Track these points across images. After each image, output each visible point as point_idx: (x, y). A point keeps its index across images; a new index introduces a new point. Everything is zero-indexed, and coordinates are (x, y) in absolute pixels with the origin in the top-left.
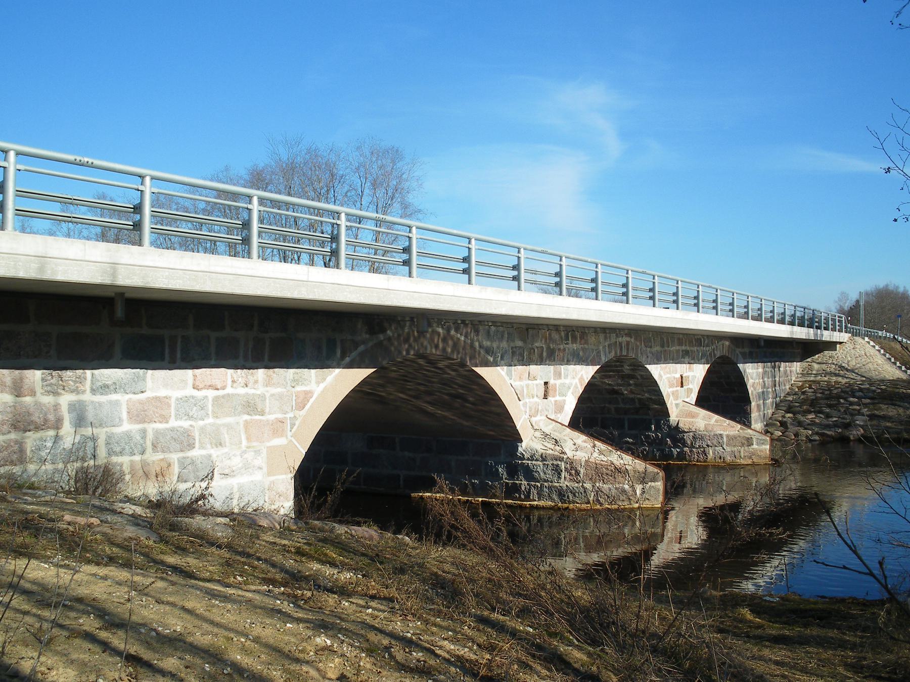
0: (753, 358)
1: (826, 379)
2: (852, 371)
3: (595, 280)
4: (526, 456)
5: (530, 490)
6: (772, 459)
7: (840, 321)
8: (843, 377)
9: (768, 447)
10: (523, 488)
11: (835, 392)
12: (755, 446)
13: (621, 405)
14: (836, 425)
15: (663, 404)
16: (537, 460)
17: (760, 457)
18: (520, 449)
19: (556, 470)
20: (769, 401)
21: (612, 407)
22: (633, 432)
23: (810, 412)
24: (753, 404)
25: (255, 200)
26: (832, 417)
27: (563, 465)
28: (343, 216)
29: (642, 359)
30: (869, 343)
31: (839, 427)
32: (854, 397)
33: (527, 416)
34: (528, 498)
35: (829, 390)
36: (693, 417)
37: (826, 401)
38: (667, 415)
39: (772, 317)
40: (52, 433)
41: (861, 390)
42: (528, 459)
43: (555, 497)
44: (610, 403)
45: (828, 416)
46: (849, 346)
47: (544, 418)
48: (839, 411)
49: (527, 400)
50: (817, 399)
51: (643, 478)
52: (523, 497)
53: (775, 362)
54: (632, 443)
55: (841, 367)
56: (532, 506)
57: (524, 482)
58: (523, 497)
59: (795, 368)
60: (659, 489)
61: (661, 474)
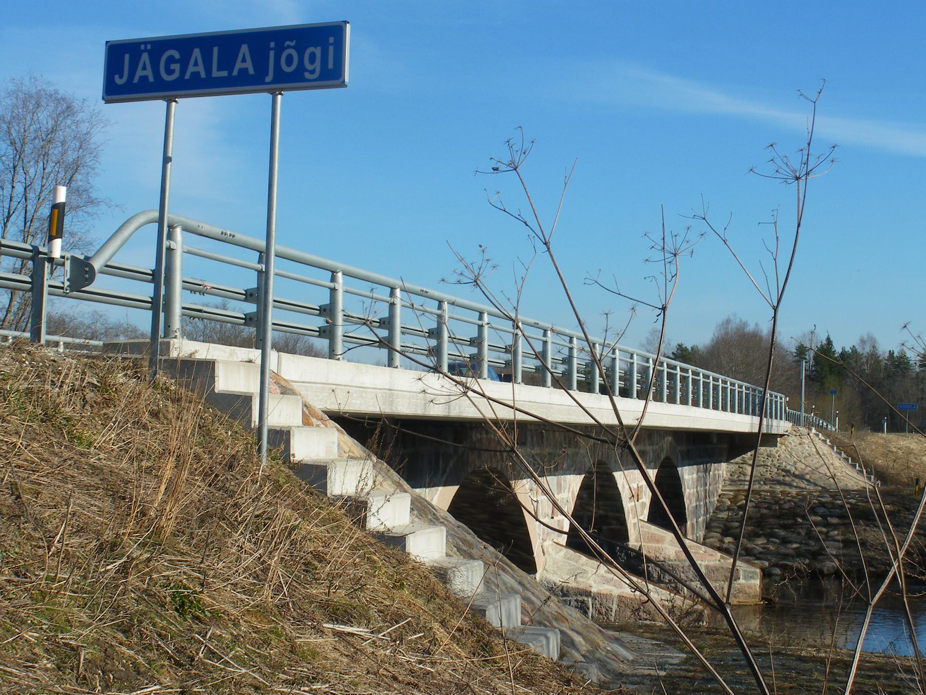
0: (690, 459)
1: (767, 487)
2: (801, 477)
3: (327, 311)
6: (763, 599)
7: (671, 377)
8: (790, 485)
9: (758, 582)
11: (787, 506)
12: (742, 581)
14: (798, 554)
15: (623, 522)
17: (748, 595)
20: (701, 519)
23: (758, 536)
24: (689, 523)
25: (665, 365)
26: (791, 542)
28: (665, 365)
30: (817, 435)
31: (806, 557)
32: (816, 514)
35: (777, 503)
36: (658, 541)
37: (777, 521)
38: (627, 538)
39: (567, 375)
41: (822, 504)
45: (785, 541)
46: (793, 441)
47: (551, 542)
48: (799, 534)
50: (763, 516)
53: (707, 463)
55: (788, 472)
59: (722, 470)
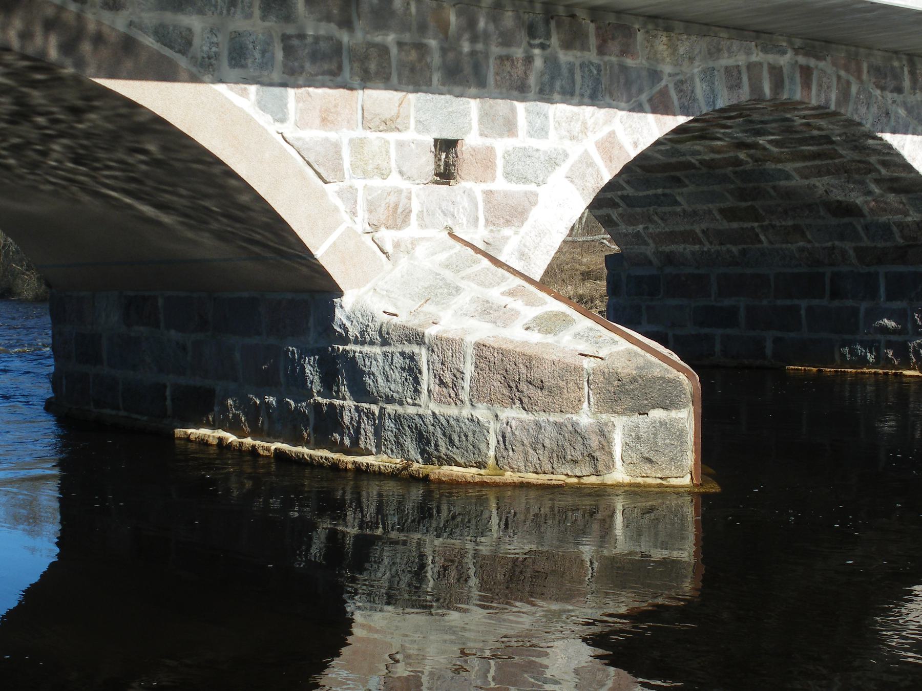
4: (353, 331)
5: (359, 423)
10: (347, 419)
13: (866, 242)
16: (372, 343)
18: (339, 314)
19: (410, 370)
21: (848, 246)
22: (898, 305)
27: (423, 356)
29: (866, 117)
33: (361, 225)
34: (355, 449)
40: (357, 354)
42: (356, 342)
43: (410, 445)
44: (842, 238)
49: (359, 184)
51: (627, 393)
52: (347, 441)
54: (895, 331)
56: (361, 472)
57: (350, 403)
58: (347, 441)
60: (681, 435)
61: (686, 381)
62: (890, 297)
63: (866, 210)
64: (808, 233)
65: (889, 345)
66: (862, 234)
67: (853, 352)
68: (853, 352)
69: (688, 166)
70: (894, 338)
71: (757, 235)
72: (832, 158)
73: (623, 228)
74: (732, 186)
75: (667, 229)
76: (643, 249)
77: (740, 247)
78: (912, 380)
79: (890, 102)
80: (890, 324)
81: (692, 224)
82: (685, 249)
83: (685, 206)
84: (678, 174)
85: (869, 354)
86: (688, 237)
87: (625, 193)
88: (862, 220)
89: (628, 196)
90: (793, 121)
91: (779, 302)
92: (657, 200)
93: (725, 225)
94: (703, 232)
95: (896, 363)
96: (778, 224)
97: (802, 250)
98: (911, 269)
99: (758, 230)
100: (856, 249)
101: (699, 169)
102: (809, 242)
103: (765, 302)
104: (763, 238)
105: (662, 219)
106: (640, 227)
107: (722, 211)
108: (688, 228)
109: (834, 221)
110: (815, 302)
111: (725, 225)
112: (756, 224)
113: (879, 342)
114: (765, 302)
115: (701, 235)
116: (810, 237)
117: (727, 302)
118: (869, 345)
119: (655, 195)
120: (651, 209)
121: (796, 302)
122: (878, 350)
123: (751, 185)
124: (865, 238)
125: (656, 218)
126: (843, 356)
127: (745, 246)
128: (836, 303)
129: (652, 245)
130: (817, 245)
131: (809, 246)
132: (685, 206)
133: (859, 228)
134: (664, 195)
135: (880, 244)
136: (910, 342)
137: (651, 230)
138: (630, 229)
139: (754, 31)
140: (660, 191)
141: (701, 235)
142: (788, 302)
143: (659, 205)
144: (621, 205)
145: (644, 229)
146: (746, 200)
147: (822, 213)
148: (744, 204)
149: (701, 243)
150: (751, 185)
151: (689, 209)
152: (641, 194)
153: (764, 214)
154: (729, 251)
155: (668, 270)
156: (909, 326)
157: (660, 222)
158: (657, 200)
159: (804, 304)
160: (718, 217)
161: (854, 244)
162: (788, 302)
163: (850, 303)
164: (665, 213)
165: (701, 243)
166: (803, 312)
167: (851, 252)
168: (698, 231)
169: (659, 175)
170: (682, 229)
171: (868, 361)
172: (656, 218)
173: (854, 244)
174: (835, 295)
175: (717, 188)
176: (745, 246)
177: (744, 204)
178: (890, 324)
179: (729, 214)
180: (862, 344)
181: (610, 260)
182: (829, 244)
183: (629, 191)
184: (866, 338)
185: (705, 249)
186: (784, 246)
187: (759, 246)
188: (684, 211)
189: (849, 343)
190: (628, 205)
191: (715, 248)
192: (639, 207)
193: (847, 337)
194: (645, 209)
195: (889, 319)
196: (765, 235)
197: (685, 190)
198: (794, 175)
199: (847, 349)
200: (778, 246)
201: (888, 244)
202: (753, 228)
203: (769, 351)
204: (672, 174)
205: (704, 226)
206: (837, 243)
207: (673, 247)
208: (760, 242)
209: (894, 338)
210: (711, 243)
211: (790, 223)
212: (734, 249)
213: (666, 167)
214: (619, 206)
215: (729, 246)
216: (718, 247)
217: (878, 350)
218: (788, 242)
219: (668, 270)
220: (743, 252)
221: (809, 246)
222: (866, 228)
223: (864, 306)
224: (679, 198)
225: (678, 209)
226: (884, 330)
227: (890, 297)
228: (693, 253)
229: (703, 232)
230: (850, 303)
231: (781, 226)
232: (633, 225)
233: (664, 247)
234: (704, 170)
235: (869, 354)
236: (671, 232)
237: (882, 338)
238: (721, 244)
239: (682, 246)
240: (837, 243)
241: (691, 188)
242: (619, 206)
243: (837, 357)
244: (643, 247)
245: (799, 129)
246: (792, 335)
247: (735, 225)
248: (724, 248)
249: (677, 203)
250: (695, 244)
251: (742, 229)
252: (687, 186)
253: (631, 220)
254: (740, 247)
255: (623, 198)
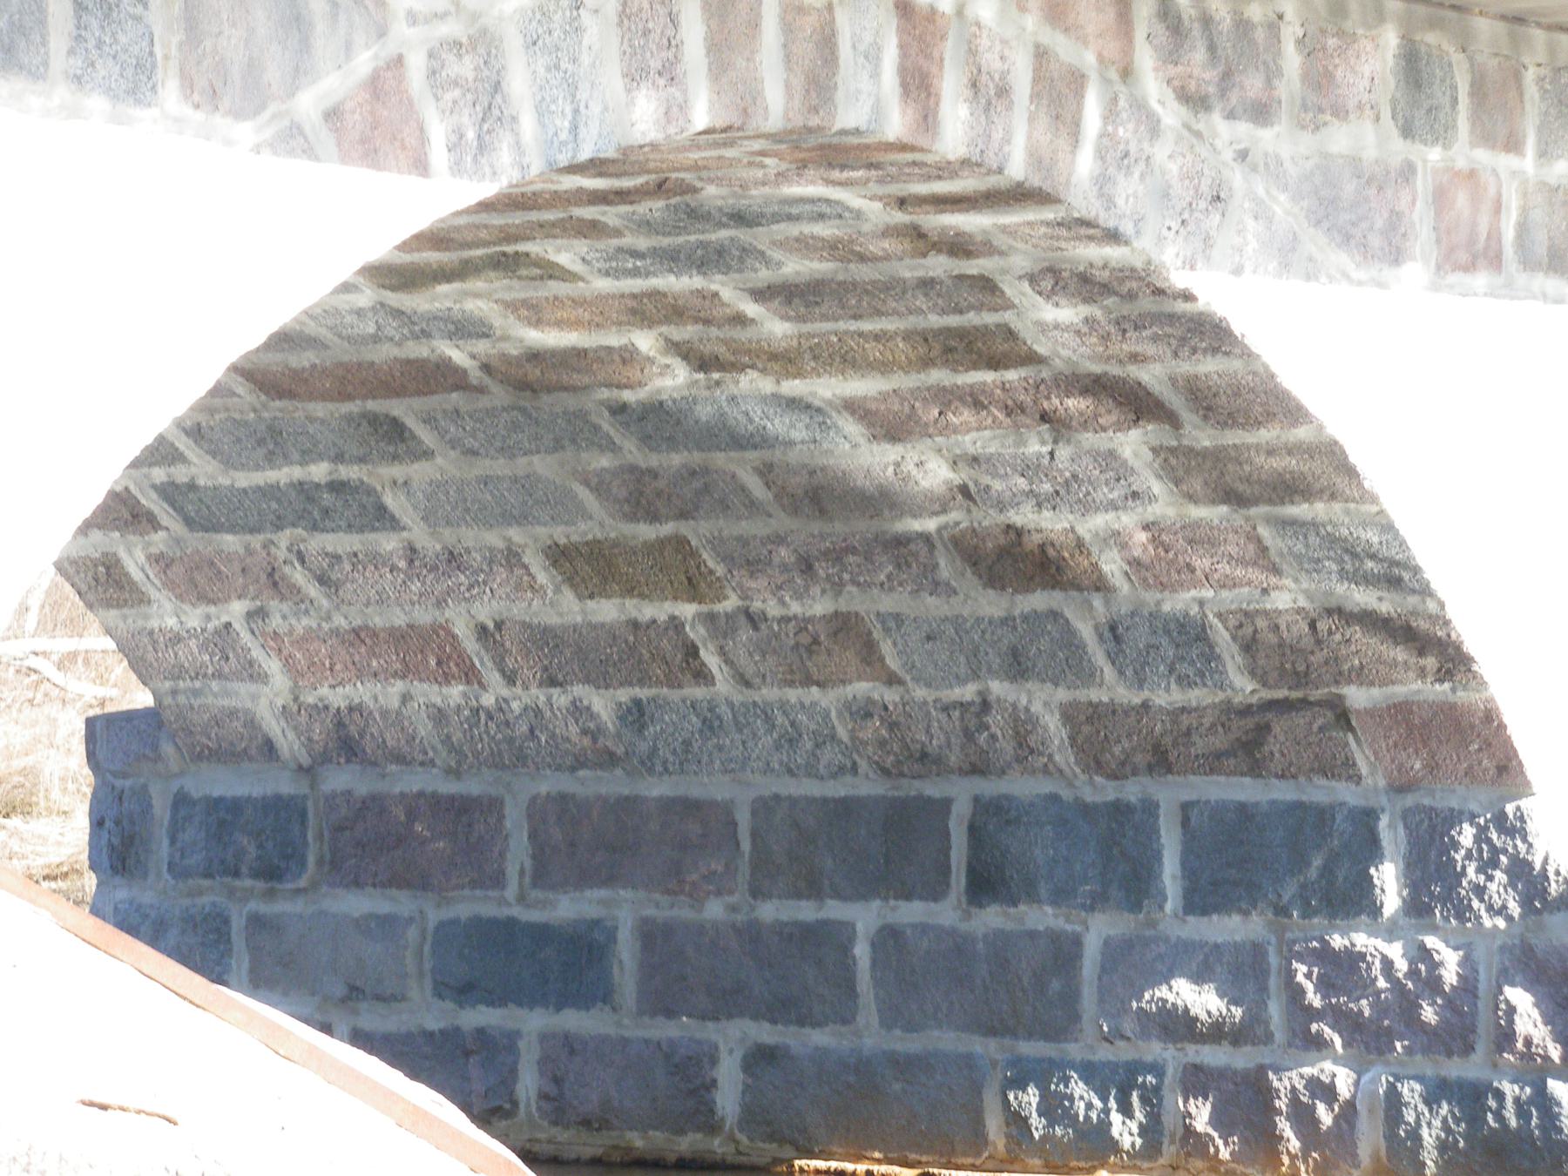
13: (1112, 689)
21: (1044, 703)
22: (1229, 928)
44: (1018, 667)
54: (1217, 1032)
62: (1199, 901)
63: (1111, 565)
64: (886, 648)
65: (1197, 1081)
66: (1100, 658)
67: (1054, 1107)
68: (1054, 1107)
69: (434, 377)
70: (1214, 1056)
71: (692, 651)
72: (995, 364)
73: (167, 614)
74: (604, 461)
75: (339, 621)
76: (241, 695)
77: (624, 695)
78: (960, 1161)
79: (1228, 155)
80: (1200, 999)
81: (440, 604)
82: (406, 698)
83: (419, 534)
84: (397, 408)
85: (1116, 1118)
86: (427, 652)
87: (181, 474)
88: (1097, 602)
89: (192, 486)
90: (695, 190)
91: (770, 911)
92: (310, 507)
93: (566, 608)
94: (482, 632)
95: (1224, 1154)
96: (773, 610)
97: (863, 711)
98: (1283, 792)
99: (696, 633)
100: (1069, 714)
101: (481, 390)
102: (892, 680)
103: (715, 910)
104: (711, 659)
105: (323, 580)
106: (236, 609)
107: (558, 556)
108: (424, 616)
109: (990, 604)
110: (911, 912)
111: (566, 608)
112: (687, 610)
113: (1157, 1069)
114: (715, 910)
115: (471, 645)
116: (893, 663)
117: (567, 908)
118: (1119, 1082)
119: (300, 486)
120: (284, 538)
121: (835, 910)
122: (1152, 1099)
123: (677, 459)
124: (1109, 672)
125: (298, 576)
126: (1017, 1120)
127: (643, 693)
128: (992, 918)
129: (279, 680)
130: (920, 693)
131: (891, 696)
132: (419, 534)
133: (1086, 631)
134: (337, 487)
135: (1167, 696)
136: (1278, 1070)
137: (276, 622)
138: (194, 618)
139: (1503, 17)
140: (319, 471)
141: (471, 645)
142: (806, 911)
143: (315, 528)
144: (165, 520)
145: (250, 615)
146: (654, 518)
147: (945, 569)
148: (646, 532)
149: (470, 675)
150: (677, 459)
151: (429, 545)
152: (245, 480)
153: (720, 570)
154: (578, 710)
155: (340, 779)
156: (1275, 1010)
157: (313, 590)
158: (310, 507)
159: (864, 918)
160: (542, 578)
161: (1062, 695)
162: (806, 911)
163: (1042, 917)
164: (337, 558)
165: (470, 675)
166: (862, 951)
167: (1052, 723)
168: (462, 629)
169: (319, 409)
170: (399, 619)
171: (1115, 1147)
172: (298, 576)
173: (1062, 695)
174: (985, 885)
175: (543, 465)
176: (643, 693)
177: (646, 532)
178: (1200, 999)
179: (588, 566)
180: (1090, 1073)
181: (107, 736)
182: (968, 692)
183: (202, 469)
184: (1104, 1054)
185: (488, 700)
186: (793, 695)
187: (699, 692)
188: (412, 551)
189: (1041, 1073)
190: (189, 522)
191: (520, 699)
192: (232, 529)
193: (1030, 1048)
194: (256, 541)
195: (1198, 978)
196: (722, 652)
197: (419, 472)
198: (841, 420)
199: (1031, 1097)
200: (770, 693)
201: (1197, 696)
202: (675, 624)
203: (728, 1100)
204: (372, 405)
205: (485, 612)
206: (997, 687)
207: (363, 692)
208: (702, 675)
209: (1214, 1056)
210: (510, 679)
211: (820, 606)
212: (603, 704)
213: (350, 380)
214: (154, 524)
215: (579, 690)
216: (538, 695)
217: (1152, 1099)
218: (808, 681)
219: (340, 779)
220: (636, 715)
221: (891, 696)
222: (1113, 632)
223: (1099, 930)
224: (389, 500)
225: (389, 543)
226: (1178, 1025)
227: (1199, 901)
228: (439, 716)
229: (482, 632)
230: (1042, 917)
231: (785, 620)
232: (204, 598)
233: (324, 691)
234: (499, 395)
235: (1116, 1118)
236: (356, 632)
237: (1171, 1056)
238: (553, 682)
239: (399, 686)
240: (997, 687)
241: (443, 465)
242: (154, 524)
243: (994, 1126)
244: (244, 689)
245: (874, 248)
246: (820, 1038)
247: (607, 610)
248: (561, 699)
249: (382, 518)
250: (447, 679)
251: (635, 625)
252: (428, 454)
253: (196, 580)
254: (624, 695)
255: (169, 492)
